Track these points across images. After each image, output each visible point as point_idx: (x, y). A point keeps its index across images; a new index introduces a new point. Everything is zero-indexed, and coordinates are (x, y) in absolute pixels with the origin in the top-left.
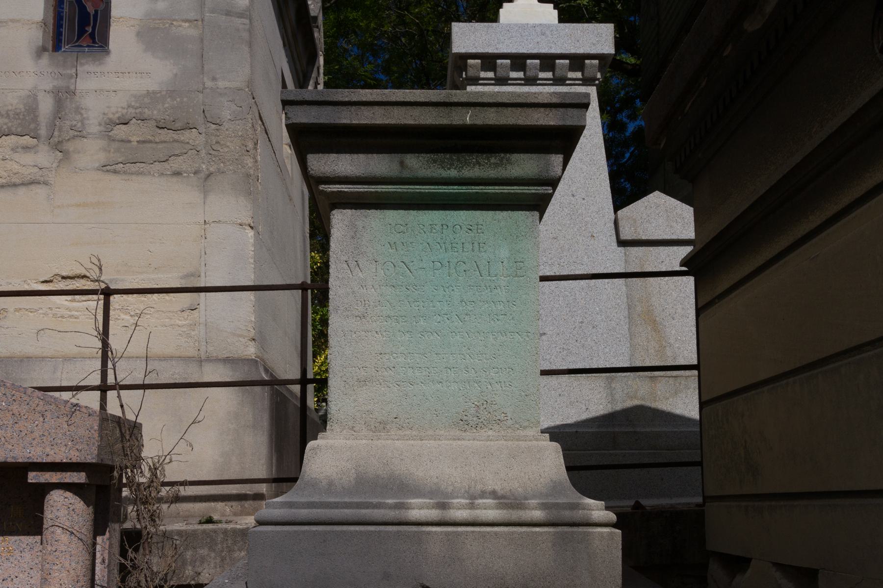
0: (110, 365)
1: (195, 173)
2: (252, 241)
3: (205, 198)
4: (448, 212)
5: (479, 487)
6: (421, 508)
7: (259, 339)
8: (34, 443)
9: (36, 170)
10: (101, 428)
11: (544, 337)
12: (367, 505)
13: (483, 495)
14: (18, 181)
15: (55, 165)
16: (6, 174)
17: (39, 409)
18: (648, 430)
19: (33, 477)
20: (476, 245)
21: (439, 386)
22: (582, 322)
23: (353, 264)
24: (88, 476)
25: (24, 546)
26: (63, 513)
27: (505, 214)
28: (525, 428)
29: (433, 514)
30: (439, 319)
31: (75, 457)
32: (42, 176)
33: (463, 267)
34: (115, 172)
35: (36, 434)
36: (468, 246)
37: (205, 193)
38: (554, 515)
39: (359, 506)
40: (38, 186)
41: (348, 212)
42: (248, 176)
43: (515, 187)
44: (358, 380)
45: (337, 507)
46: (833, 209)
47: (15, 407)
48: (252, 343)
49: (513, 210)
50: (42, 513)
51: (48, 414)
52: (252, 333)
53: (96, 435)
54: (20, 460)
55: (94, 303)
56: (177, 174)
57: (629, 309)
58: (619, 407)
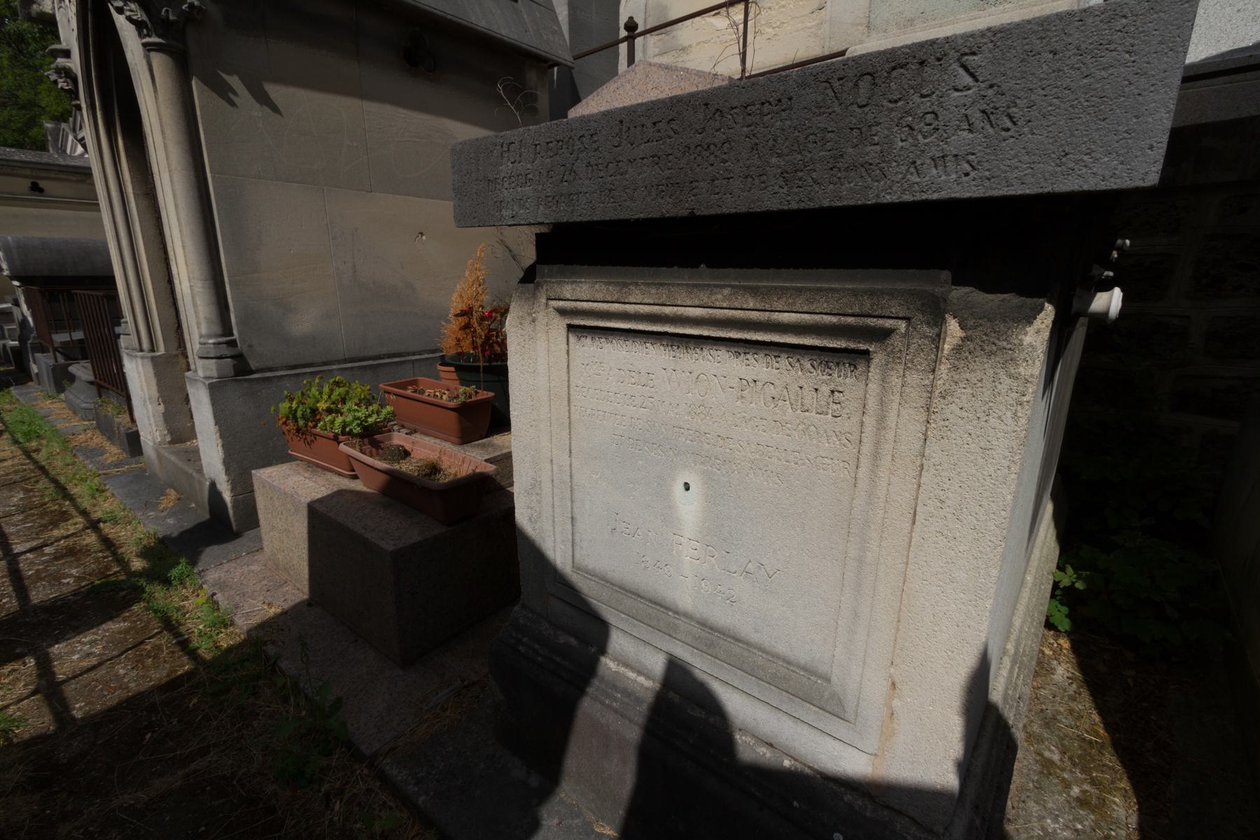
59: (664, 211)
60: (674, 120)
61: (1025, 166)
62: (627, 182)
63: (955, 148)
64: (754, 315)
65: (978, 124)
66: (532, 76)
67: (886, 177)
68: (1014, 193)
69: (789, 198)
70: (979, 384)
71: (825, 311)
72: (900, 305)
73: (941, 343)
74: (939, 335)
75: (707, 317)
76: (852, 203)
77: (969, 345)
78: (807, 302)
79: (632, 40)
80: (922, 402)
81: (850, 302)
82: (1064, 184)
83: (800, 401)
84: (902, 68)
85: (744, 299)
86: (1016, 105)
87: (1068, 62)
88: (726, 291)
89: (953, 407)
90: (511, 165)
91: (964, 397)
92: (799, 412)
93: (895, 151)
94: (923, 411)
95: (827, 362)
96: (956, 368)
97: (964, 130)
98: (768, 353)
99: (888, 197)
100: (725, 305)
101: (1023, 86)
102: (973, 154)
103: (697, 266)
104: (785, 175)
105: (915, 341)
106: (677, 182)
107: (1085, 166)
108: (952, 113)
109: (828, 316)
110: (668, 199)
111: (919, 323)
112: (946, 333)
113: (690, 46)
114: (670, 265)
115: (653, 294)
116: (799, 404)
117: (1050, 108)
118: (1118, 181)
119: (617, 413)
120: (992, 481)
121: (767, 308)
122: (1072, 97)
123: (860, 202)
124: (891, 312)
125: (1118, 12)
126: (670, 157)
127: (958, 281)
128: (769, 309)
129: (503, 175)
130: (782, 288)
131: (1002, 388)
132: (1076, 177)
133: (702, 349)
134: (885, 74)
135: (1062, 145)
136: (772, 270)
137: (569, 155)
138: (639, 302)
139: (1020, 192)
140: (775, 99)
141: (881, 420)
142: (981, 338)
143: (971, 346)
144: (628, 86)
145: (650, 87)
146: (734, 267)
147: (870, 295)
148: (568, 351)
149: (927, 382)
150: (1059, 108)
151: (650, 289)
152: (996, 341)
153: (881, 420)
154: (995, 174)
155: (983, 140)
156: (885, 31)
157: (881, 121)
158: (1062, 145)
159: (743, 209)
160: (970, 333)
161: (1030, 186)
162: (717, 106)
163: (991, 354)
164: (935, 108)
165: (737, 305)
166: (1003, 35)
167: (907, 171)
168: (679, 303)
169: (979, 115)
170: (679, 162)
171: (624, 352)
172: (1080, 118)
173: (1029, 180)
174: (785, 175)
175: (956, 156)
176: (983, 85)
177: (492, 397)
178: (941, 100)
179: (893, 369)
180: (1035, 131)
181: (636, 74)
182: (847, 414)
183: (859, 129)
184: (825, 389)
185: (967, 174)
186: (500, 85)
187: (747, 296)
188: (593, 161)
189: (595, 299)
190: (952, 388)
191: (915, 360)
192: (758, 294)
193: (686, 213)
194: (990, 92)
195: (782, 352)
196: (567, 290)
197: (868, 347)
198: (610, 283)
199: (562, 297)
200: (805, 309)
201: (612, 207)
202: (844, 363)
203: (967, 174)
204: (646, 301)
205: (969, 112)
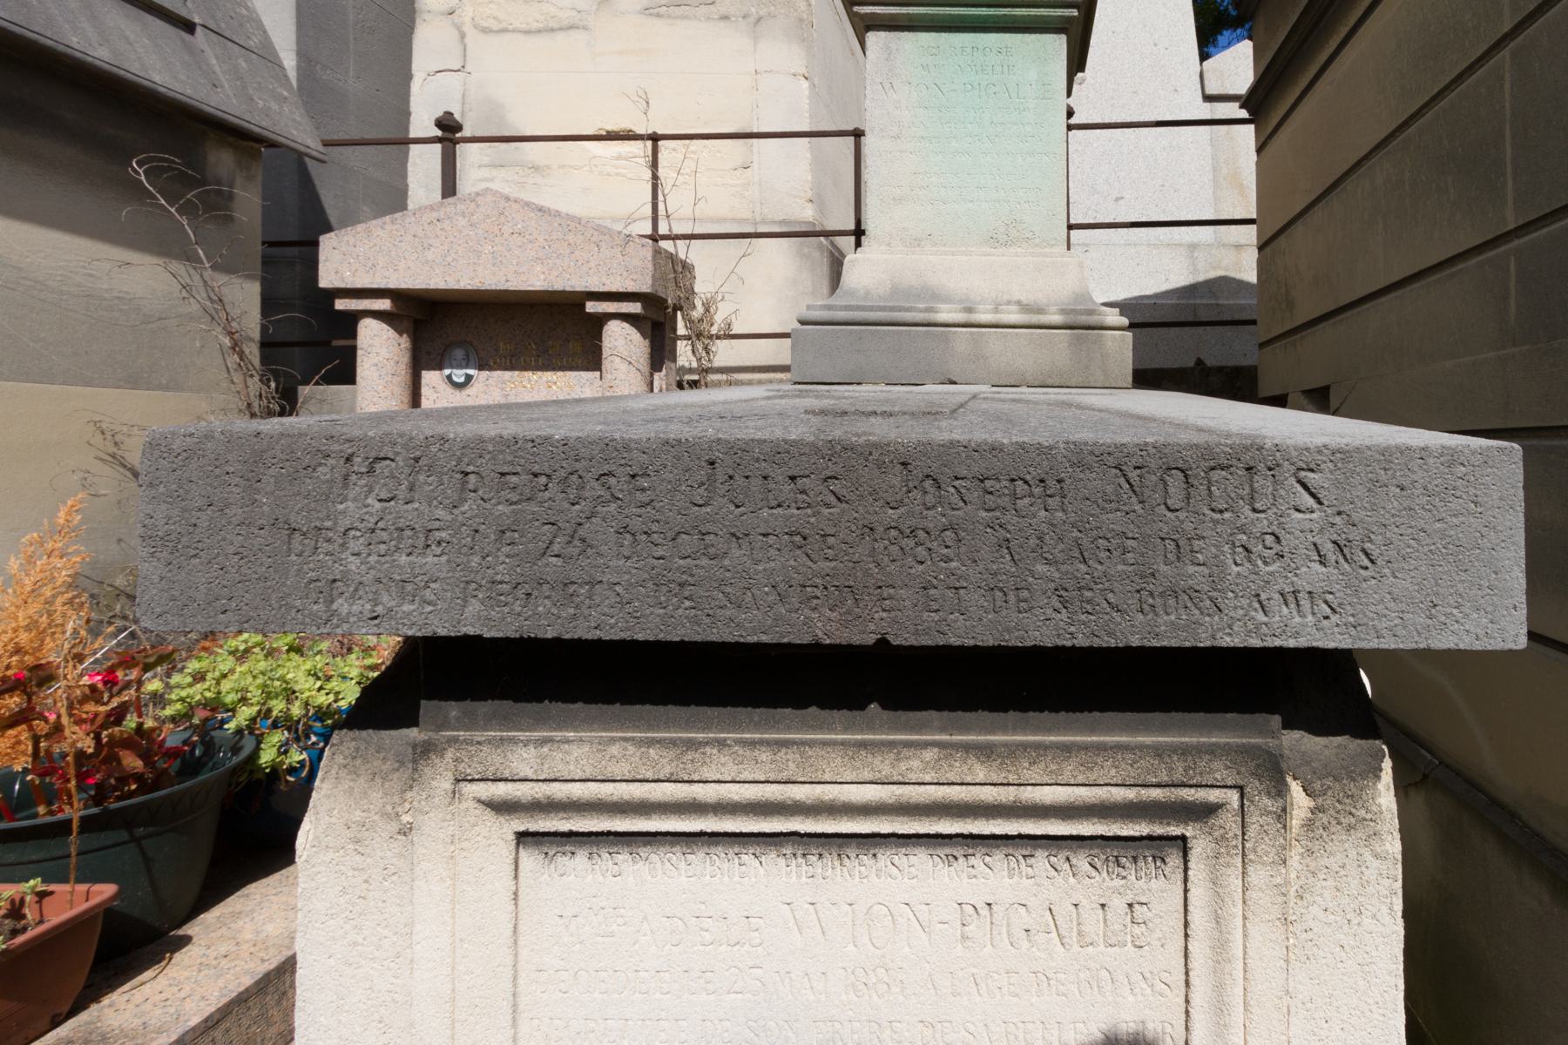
0: (661, 197)
1: (744, 17)
2: (807, 93)
3: (755, 45)
4: (978, 35)
5: (1006, 297)
6: (950, 312)
7: (817, 200)
8: (591, 272)
9: (574, 13)
10: (654, 258)
11: (1121, 202)
12: (900, 309)
13: (1009, 303)
14: (555, 25)
15: (594, 8)
16: (542, 18)
17: (594, 239)
18: (1231, 302)
19: (592, 307)
20: (1005, 67)
21: (970, 205)
22: (1163, 186)
23: (887, 86)
24: (643, 308)
25: (584, 381)
26: (621, 343)
27: (1033, 36)
28: (1052, 245)
29: (960, 317)
30: (970, 140)
31: (631, 287)
32: (581, 20)
33: (993, 89)
34: (658, 15)
35: (592, 264)
36: (998, 69)
37: (756, 39)
38: (1070, 319)
39: (892, 309)
40: (576, 31)
41: (882, 34)
42: (801, 20)
43: (1042, 10)
44: (894, 199)
45: (871, 310)
46: (1344, 31)
47: (571, 237)
48: (810, 205)
49: (1041, 33)
50: (601, 341)
51: (603, 245)
52: (809, 194)
53: (650, 266)
54: (578, 289)
55: (641, 149)
56: (725, 18)
57: (1214, 171)
58: (1201, 278)
59: (820, 634)
60: (837, 479)
61: (1393, 615)
62: (728, 574)
63: (1308, 583)
64: (988, 794)
65: (1332, 557)
66: (221, 161)
67: (1220, 610)
68: (1386, 646)
69: (1072, 629)
70: (1343, 872)
71: (1114, 781)
72: (1227, 768)
73: (1288, 820)
74: (1284, 810)
75: (890, 801)
76: (1174, 643)
77: (1321, 818)
78: (1082, 768)
79: (451, 145)
80: (1276, 912)
81: (1152, 765)
82: (1440, 641)
83: (1075, 929)
84: (1222, 469)
85: (965, 768)
86: (1371, 541)
87: (1417, 501)
88: (929, 754)
89: (1315, 910)
90: (378, 505)
91: (1327, 894)
92: (1076, 948)
93: (1229, 577)
94: (1280, 925)
95: (1116, 857)
96: (1310, 852)
97: (1314, 561)
98: (1011, 851)
99: (1228, 639)
100: (928, 778)
101: (1374, 519)
102: (1331, 593)
103: (861, 706)
104: (1062, 593)
105: (1254, 819)
106: (847, 584)
107: (1457, 622)
108: (1298, 538)
109: (1118, 788)
110: (828, 613)
111: (1256, 793)
112: (1292, 804)
113: (548, 167)
114: (800, 703)
115: (764, 762)
116: (1075, 934)
117: (1408, 550)
118: (1492, 641)
119: (663, 1014)
120: (1381, 1011)
121: (1011, 781)
122: (1428, 541)
123: (1188, 644)
124: (1216, 779)
125: (1455, 458)
126: (831, 540)
127: (1288, 725)
128: (1015, 782)
129: (345, 523)
130: (1038, 746)
131: (1371, 874)
132: (1450, 633)
133: (874, 855)
134: (1202, 474)
135: (1428, 595)
136: (1011, 713)
137: (567, 505)
138: (729, 779)
139: (1393, 646)
140: (1033, 478)
141: (1220, 946)
142: (1335, 808)
143: (1325, 820)
144: (462, 222)
145: (507, 229)
146: (939, 708)
147: (1181, 754)
148: (516, 894)
149: (1279, 880)
150: (1418, 551)
151: (757, 752)
152: (1354, 811)
153: (1220, 946)
154: (1361, 622)
155: (1340, 577)
156: (889, 245)
157: (1205, 534)
158: (1428, 595)
159: (988, 640)
160: (1320, 800)
161: (1403, 639)
162: (927, 471)
163: (1350, 828)
164: (1274, 528)
165: (952, 777)
166: (1342, 456)
167: (1250, 605)
168: (827, 777)
169: (1330, 546)
170: (851, 551)
171: (683, 879)
172: (1441, 566)
173: (1401, 632)
174: (1062, 593)
175: (1310, 593)
176: (1329, 511)
177: (113, 898)
178: (1282, 520)
179: (1228, 865)
180: (1397, 574)
181: (478, 206)
182: (1159, 939)
183: (1174, 540)
184: (1118, 904)
185: (1327, 618)
186: (140, 164)
187: (972, 760)
188: (636, 525)
189: (609, 776)
190: (1309, 881)
191: (1259, 849)
192: (994, 756)
193: (870, 639)
194: (1338, 520)
195: (1035, 848)
196: (524, 760)
197: (1184, 831)
198: (651, 743)
199: (507, 774)
200: (1081, 779)
201: (686, 617)
202: (1145, 857)
203: (1327, 618)
204: (746, 776)
205: (1317, 540)
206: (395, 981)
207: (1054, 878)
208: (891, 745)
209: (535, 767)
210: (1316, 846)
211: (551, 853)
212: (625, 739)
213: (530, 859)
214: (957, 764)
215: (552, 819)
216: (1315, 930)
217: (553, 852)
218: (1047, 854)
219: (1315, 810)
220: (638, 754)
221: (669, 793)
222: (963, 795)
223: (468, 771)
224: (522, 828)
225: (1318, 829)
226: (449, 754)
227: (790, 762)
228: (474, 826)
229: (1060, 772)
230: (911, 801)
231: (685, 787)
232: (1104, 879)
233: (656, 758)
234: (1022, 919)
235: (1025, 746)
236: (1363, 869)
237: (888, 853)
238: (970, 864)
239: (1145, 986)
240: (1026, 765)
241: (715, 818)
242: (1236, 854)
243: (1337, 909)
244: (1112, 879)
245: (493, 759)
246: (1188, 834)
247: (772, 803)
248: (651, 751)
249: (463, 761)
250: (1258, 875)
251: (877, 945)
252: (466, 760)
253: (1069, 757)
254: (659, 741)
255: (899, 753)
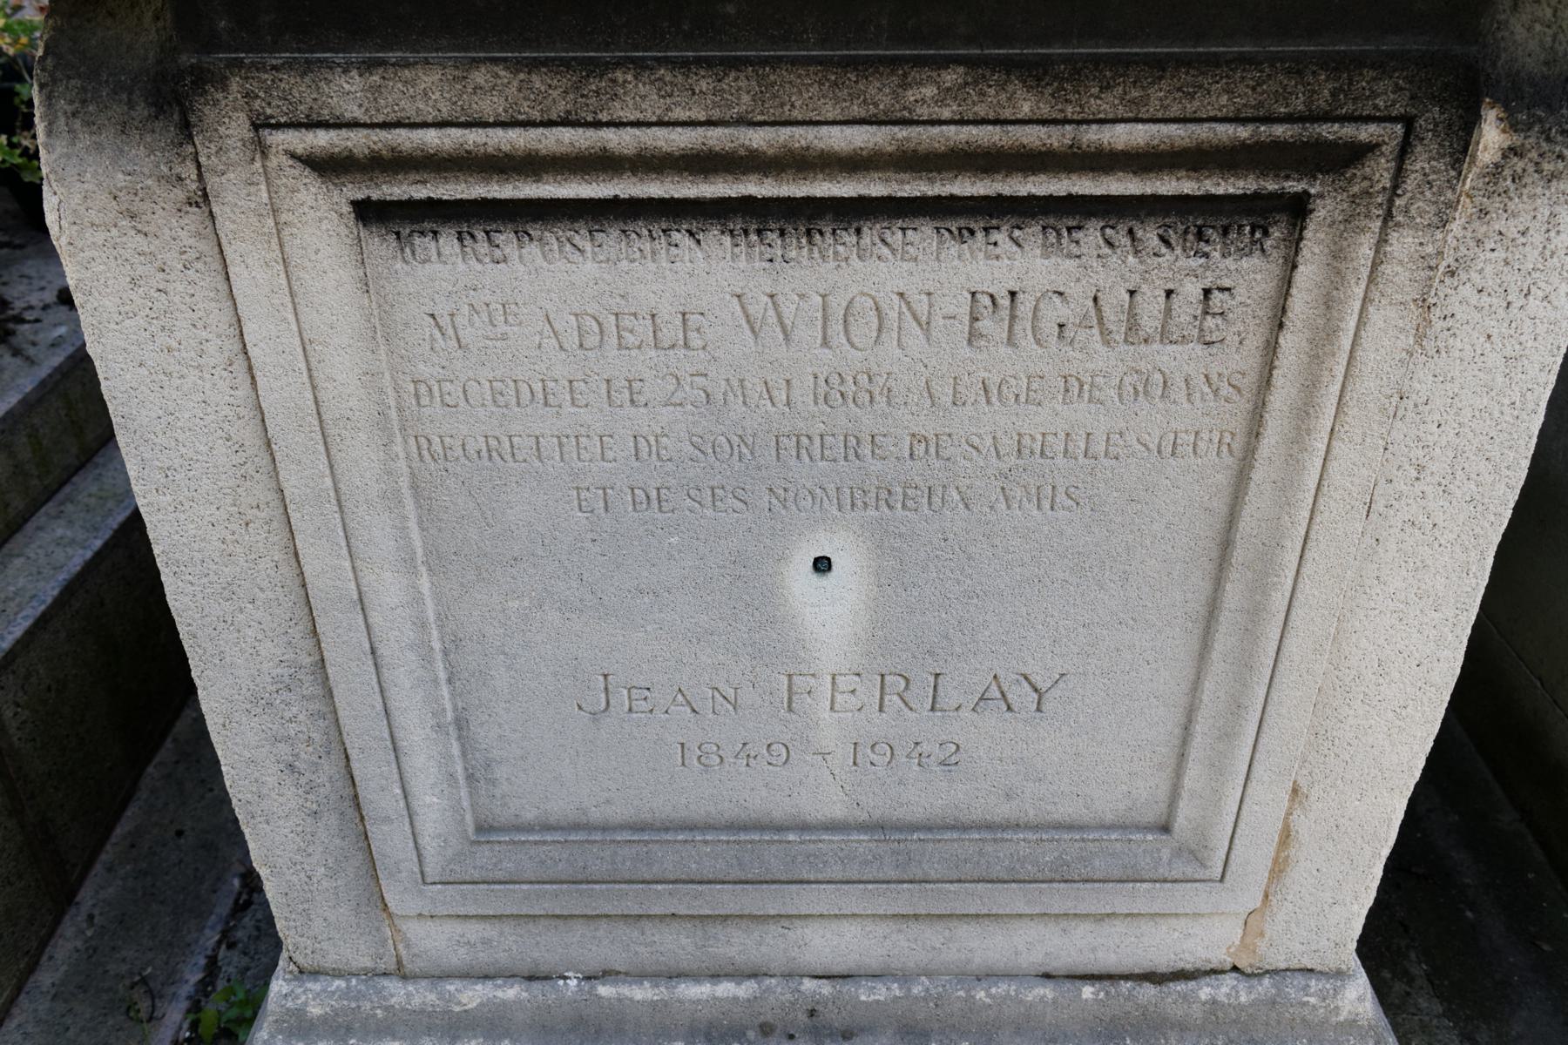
64: (1033, 136)
70: (1523, 240)
88: (950, 77)
91: (1489, 269)
100: (946, 114)
124: (1376, 107)
147: (1335, 69)
149: (1430, 249)
153: (1323, 337)
165: (981, 110)
168: (797, 114)
187: (1016, 86)
192: (1047, 79)
198: (533, 65)
199: (325, 114)
200: (1175, 111)
202: (1241, 227)
204: (679, 114)
206: (232, 392)
207: (1107, 256)
208: (894, 62)
209: (366, 104)
210: (1495, 204)
211: (405, 232)
212: (495, 61)
213: (379, 246)
214: (992, 91)
215: (401, 183)
216: (1458, 317)
217: (408, 231)
218: (1102, 224)
219: (1512, 151)
220: (515, 83)
221: (567, 141)
222: (997, 138)
223: (269, 111)
224: (360, 196)
225: (1505, 180)
226: (235, 84)
227: (741, 92)
228: (293, 192)
229: (1143, 101)
230: (921, 148)
231: (590, 132)
232: (1177, 257)
233: (543, 89)
234: (1055, 311)
235: (1097, 61)
236: (1552, 234)
237: (878, 226)
238: (992, 240)
239: (1206, 389)
240: (1095, 90)
241: (634, 179)
242: (1378, 216)
243: (1497, 288)
244: (1189, 257)
245: (302, 92)
246: (1313, 191)
247: (717, 154)
248: (534, 77)
249: (257, 97)
250: (1403, 243)
251: (855, 340)
252: (262, 94)
253: (1161, 78)
254: (545, 62)
255: (905, 75)
